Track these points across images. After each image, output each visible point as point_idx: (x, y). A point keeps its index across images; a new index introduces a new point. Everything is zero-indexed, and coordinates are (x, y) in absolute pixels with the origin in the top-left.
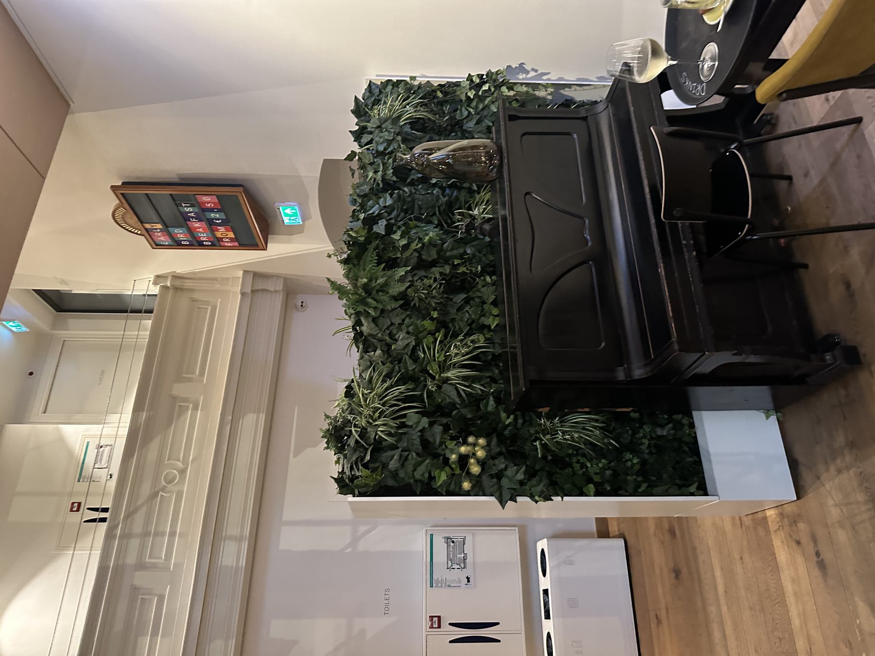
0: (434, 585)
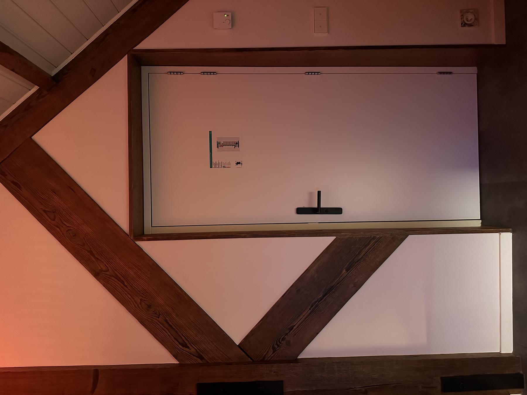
0: (213, 166)
